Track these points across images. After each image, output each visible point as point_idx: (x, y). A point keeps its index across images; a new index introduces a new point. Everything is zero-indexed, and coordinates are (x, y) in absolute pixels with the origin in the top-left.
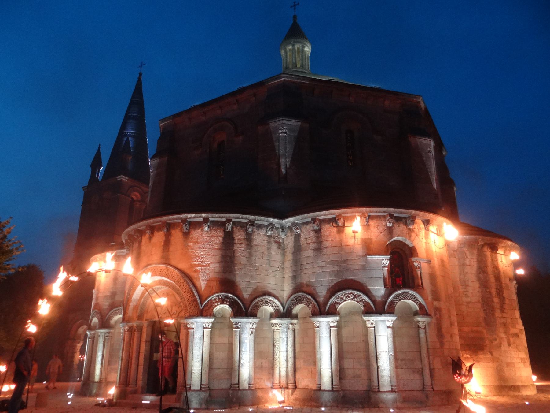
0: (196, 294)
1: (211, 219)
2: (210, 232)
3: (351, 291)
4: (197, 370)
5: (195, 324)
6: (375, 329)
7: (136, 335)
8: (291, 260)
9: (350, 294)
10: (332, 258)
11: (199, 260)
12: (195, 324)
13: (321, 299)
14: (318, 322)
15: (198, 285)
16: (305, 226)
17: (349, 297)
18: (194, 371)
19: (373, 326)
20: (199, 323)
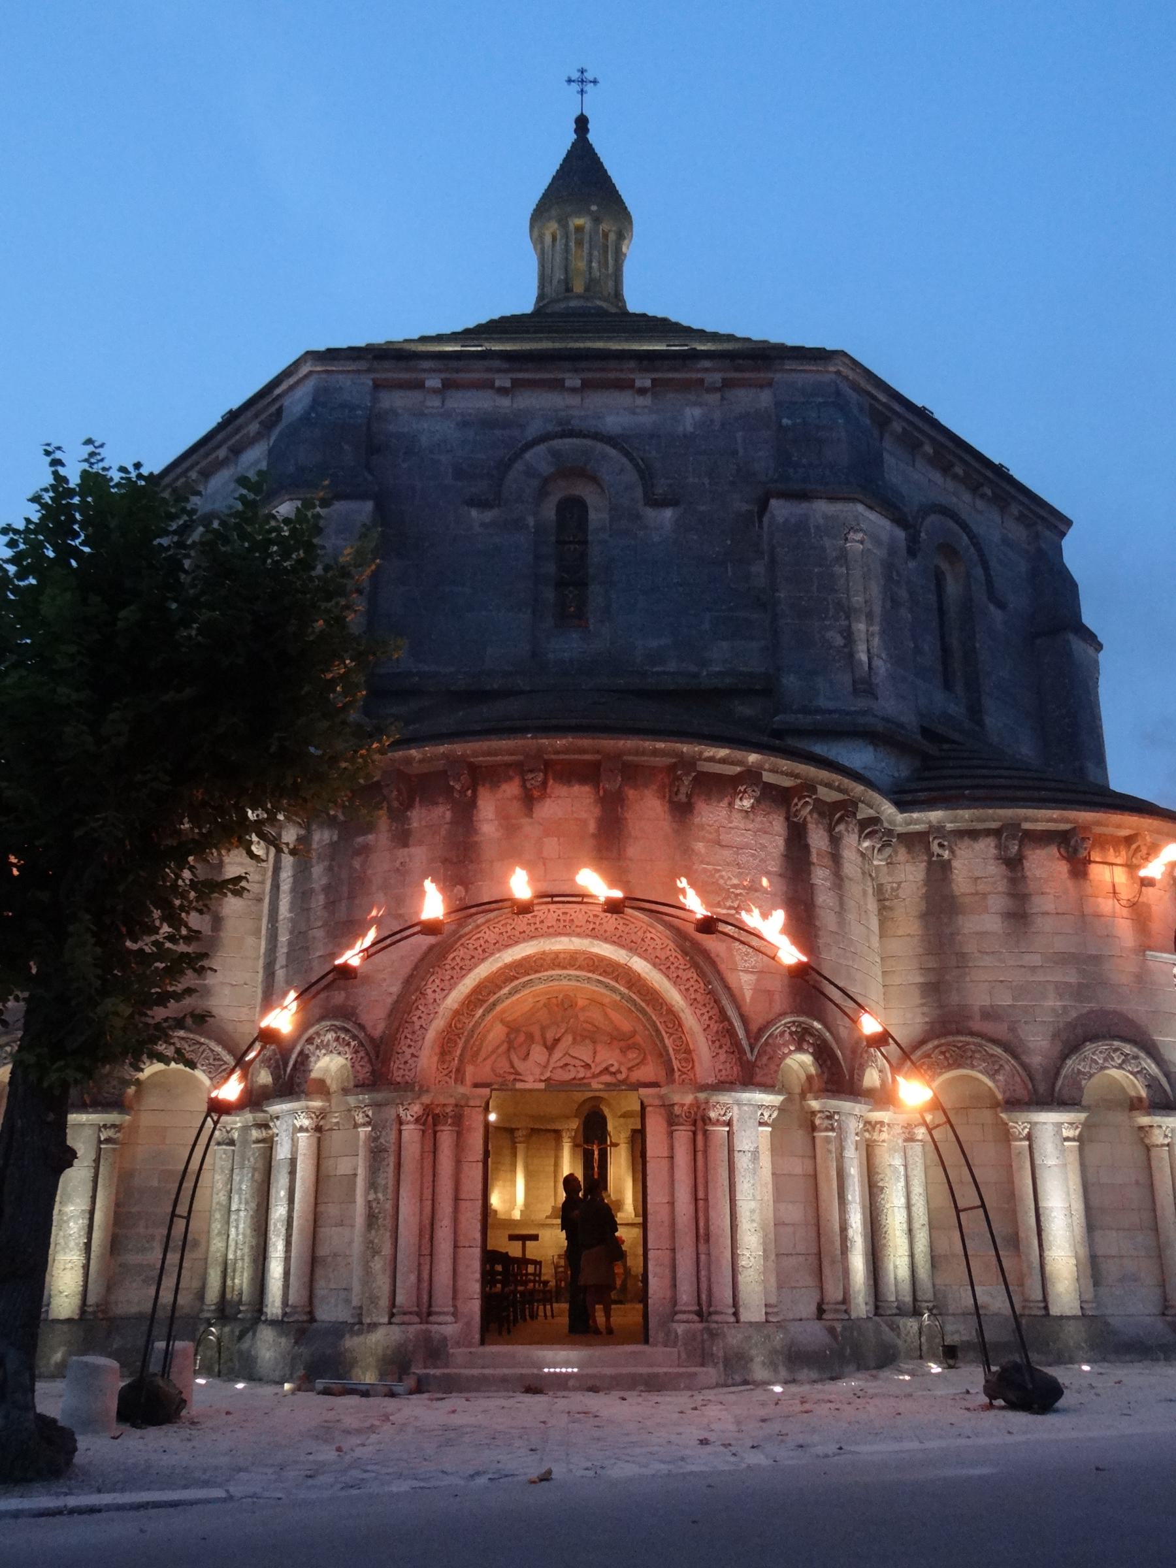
0: (731, 1012)
1: (768, 777)
2: (751, 815)
3: (1116, 1043)
4: (752, 1259)
5: (736, 1108)
6: (1030, 1146)
7: (446, 1138)
8: (914, 936)
9: (1116, 1050)
10: (1060, 945)
11: (729, 903)
12: (736, 1108)
13: (1036, 1060)
14: (1030, 1123)
15: (733, 982)
16: (967, 841)
17: (1113, 1059)
18: (743, 1263)
19: (1166, 1141)
20: (746, 1108)
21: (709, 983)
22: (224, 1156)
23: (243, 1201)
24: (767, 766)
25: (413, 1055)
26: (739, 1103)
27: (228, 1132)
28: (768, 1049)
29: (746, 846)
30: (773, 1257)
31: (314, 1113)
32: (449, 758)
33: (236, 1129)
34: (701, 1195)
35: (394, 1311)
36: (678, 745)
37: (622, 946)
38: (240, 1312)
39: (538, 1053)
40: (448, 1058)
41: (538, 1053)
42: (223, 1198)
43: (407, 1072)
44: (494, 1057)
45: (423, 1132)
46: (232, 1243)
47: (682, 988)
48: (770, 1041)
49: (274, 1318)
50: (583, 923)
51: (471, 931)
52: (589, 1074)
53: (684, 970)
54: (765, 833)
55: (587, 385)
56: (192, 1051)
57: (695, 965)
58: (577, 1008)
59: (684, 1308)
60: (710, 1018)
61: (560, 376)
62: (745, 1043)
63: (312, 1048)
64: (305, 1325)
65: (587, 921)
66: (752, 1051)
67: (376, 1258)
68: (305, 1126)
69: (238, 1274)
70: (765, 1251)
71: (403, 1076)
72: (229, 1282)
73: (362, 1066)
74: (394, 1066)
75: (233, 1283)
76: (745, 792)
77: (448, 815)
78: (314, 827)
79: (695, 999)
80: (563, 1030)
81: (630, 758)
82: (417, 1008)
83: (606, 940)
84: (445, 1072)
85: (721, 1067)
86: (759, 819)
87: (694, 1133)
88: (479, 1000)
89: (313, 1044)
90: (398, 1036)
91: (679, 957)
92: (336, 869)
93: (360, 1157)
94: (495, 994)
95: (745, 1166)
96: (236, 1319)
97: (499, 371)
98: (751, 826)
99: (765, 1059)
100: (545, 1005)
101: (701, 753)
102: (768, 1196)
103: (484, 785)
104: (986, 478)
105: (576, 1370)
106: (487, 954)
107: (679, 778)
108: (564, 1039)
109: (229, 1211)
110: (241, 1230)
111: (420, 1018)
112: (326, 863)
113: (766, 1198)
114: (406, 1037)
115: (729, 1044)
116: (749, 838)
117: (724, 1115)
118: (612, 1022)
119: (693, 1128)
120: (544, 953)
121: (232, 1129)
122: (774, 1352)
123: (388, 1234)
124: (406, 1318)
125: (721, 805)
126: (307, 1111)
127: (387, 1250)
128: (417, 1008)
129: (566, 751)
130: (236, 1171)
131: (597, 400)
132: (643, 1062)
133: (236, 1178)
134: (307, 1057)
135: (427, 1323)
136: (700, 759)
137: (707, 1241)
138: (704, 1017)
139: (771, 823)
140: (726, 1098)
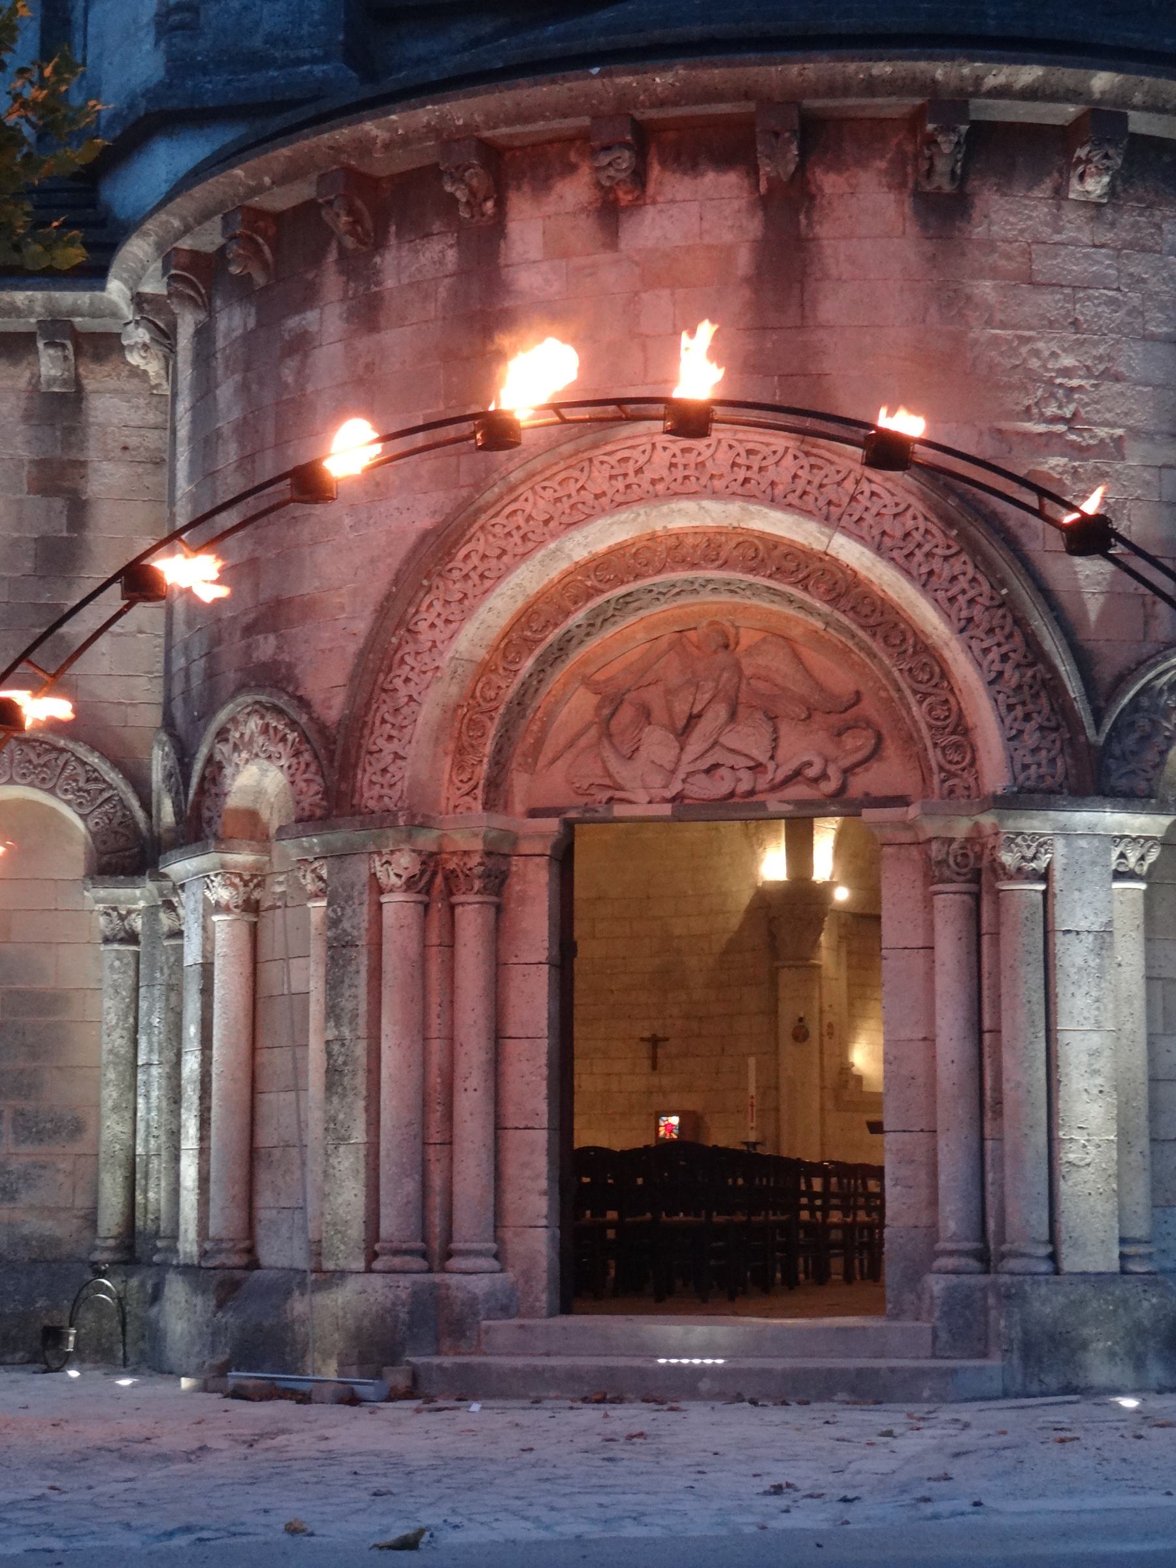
0: (1052, 643)
1: (1140, 123)
2: (1109, 214)
5: (1060, 844)
11: (1051, 410)
12: (1060, 844)
18: (1072, 1157)
20: (1083, 843)
21: (1003, 583)
22: (117, 963)
23: (156, 1045)
24: (1138, 98)
25: (397, 756)
26: (1067, 834)
27: (122, 918)
28: (1143, 722)
29: (1099, 281)
30: (1143, 1143)
31: (240, 875)
32: (442, 134)
33: (139, 912)
34: (987, 1023)
35: (377, 1247)
36: (922, 65)
37: (808, 513)
38: (157, 1250)
40: (471, 759)
42: (119, 1041)
43: (386, 791)
44: (569, 756)
45: (427, 907)
46: (141, 1126)
47: (941, 595)
48: (1145, 702)
49: (188, 1261)
50: (726, 469)
51: (501, 497)
52: (763, 782)
53: (946, 558)
54: (1144, 249)
56: (45, 765)
57: (970, 546)
58: (741, 648)
59: (468, 1246)
60: (1004, 658)
62: (1082, 708)
63: (226, 748)
64: (239, 1274)
65: (734, 465)
66: (1098, 724)
67: (342, 1149)
68: (223, 902)
69: (152, 1183)
70: (1122, 1132)
71: (381, 797)
72: (139, 1198)
73: (306, 781)
74: (363, 779)
75: (146, 1198)
76: (1088, 161)
77: (451, 255)
78: (218, 303)
79: (970, 620)
80: (707, 696)
81: (818, 103)
83: (773, 502)
84: (466, 788)
85: (1028, 760)
86: (1126, 219)
87: (977, 897)
88: (526, 639)
89: (226, 740)
90: (369, 718)
91: (935, 530)
92: (255, 387)
93: (312, 959)
94: (556, 625)
95: (1079, 961)
96: (151, 1264)
98: (1107, 237)
99: (1131, 741)
100: (672, 646)
101: (978, 80)
102: (1135, 1022)
103: (519, 188)
105: (720, 1361)
106: (530, 545)
107: (931, 141)
108: (709, 715)
109: (135, 1066)
110: (154, 1101)
111: (407, 680)
112: (238, 377)
113: (1128, 1026)
114: (384, 721)
115: (1046, 710)
116: (1103, 264)
117: (1034, 858)
119: (972, 887)
120: (653, 537)
121: (129, 912)
122: (1139, 1331)
123: (361, 1104)
124: (397, 1261)
125: (1037, 193)
126: (225, 870)
127: (359, 1135)
128: (402, 661)
129: (677, 97)
130: (142, 991)
132: (876, 753)
133: (143, 1005)
134: (220, 767)
135: (444, 1270)
136: (976, 94)
137: (998, 1113)
138: (991, 656)
139: (1158, 227)
140: (1037, 823)
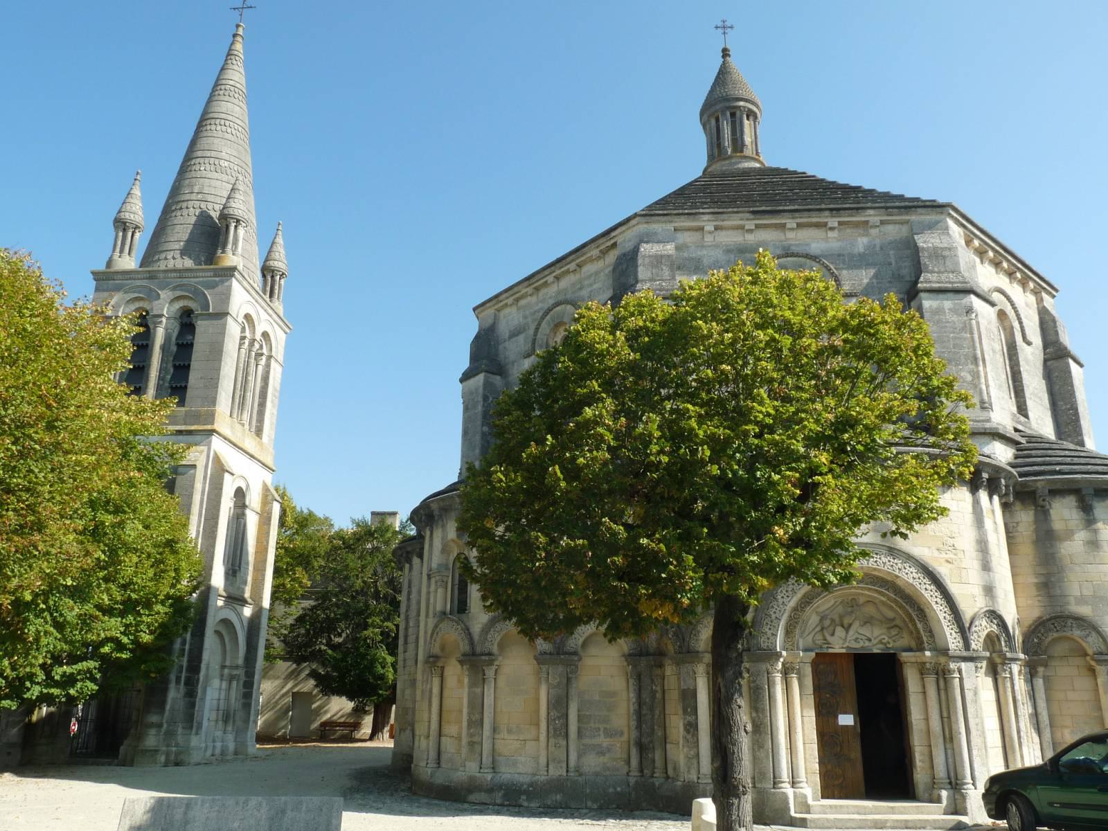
25: (773, 634)
34: (945, 715)
39: (840, 632)
41: (840, 632)
55: (800, 226)
61: (783, 221)
82: (773, 607)
97: (748, 219)
104: (1018, 268)
118: (881, 613)
131: (804, 235)
